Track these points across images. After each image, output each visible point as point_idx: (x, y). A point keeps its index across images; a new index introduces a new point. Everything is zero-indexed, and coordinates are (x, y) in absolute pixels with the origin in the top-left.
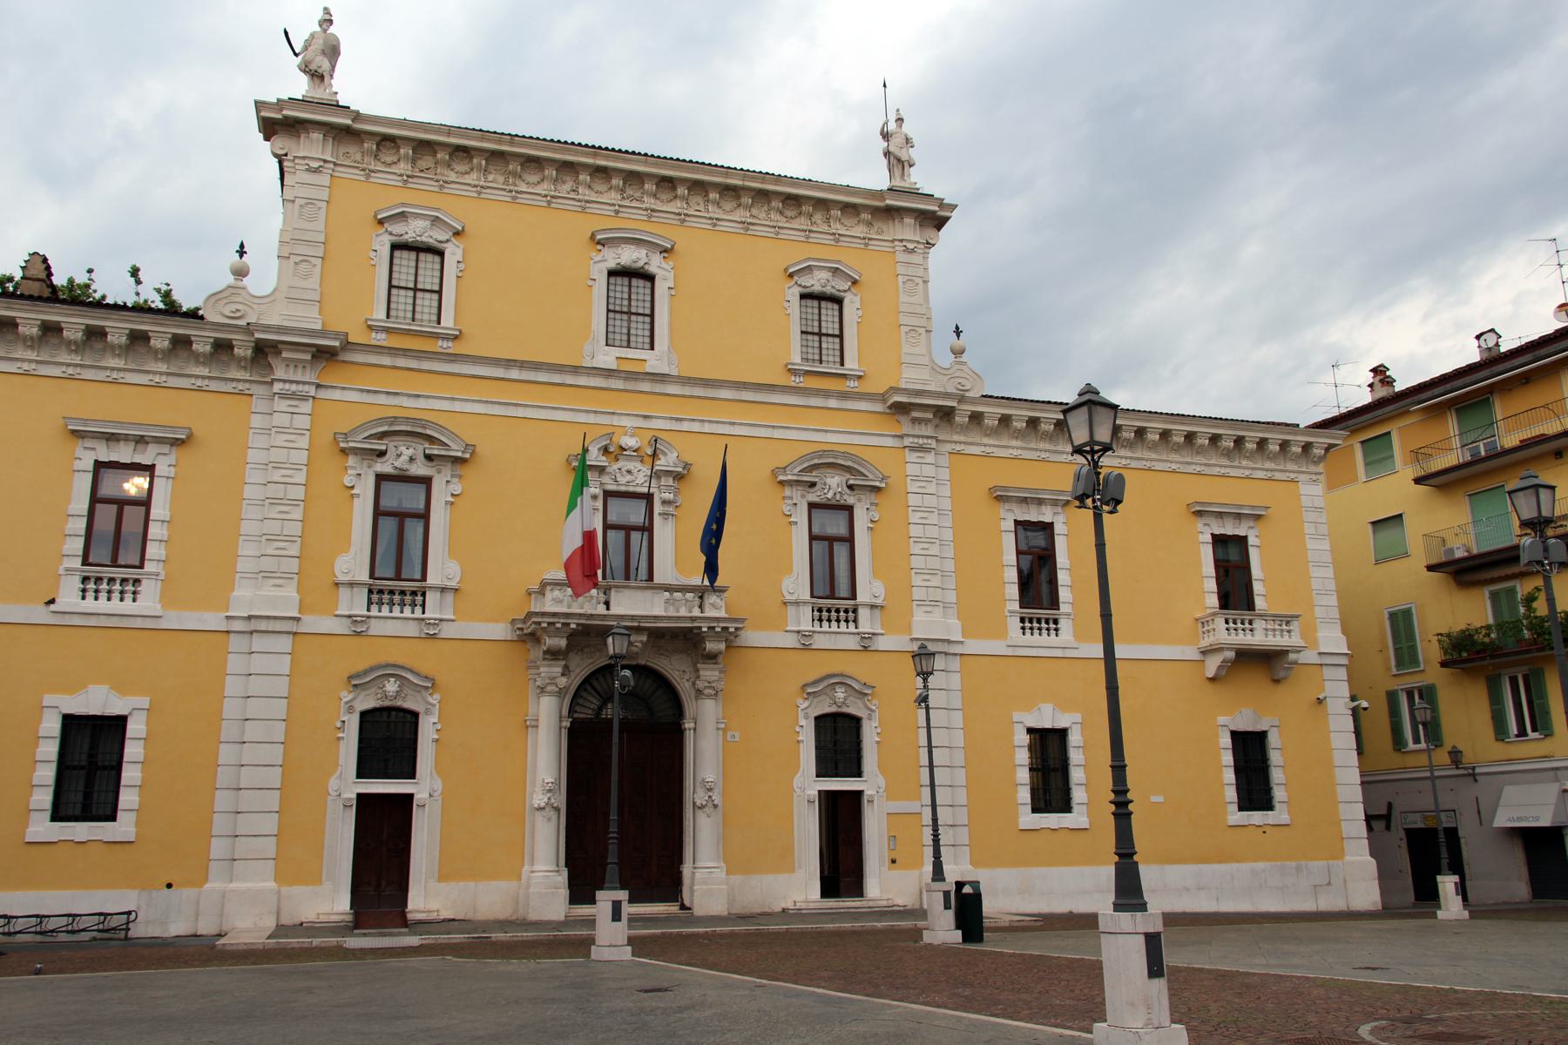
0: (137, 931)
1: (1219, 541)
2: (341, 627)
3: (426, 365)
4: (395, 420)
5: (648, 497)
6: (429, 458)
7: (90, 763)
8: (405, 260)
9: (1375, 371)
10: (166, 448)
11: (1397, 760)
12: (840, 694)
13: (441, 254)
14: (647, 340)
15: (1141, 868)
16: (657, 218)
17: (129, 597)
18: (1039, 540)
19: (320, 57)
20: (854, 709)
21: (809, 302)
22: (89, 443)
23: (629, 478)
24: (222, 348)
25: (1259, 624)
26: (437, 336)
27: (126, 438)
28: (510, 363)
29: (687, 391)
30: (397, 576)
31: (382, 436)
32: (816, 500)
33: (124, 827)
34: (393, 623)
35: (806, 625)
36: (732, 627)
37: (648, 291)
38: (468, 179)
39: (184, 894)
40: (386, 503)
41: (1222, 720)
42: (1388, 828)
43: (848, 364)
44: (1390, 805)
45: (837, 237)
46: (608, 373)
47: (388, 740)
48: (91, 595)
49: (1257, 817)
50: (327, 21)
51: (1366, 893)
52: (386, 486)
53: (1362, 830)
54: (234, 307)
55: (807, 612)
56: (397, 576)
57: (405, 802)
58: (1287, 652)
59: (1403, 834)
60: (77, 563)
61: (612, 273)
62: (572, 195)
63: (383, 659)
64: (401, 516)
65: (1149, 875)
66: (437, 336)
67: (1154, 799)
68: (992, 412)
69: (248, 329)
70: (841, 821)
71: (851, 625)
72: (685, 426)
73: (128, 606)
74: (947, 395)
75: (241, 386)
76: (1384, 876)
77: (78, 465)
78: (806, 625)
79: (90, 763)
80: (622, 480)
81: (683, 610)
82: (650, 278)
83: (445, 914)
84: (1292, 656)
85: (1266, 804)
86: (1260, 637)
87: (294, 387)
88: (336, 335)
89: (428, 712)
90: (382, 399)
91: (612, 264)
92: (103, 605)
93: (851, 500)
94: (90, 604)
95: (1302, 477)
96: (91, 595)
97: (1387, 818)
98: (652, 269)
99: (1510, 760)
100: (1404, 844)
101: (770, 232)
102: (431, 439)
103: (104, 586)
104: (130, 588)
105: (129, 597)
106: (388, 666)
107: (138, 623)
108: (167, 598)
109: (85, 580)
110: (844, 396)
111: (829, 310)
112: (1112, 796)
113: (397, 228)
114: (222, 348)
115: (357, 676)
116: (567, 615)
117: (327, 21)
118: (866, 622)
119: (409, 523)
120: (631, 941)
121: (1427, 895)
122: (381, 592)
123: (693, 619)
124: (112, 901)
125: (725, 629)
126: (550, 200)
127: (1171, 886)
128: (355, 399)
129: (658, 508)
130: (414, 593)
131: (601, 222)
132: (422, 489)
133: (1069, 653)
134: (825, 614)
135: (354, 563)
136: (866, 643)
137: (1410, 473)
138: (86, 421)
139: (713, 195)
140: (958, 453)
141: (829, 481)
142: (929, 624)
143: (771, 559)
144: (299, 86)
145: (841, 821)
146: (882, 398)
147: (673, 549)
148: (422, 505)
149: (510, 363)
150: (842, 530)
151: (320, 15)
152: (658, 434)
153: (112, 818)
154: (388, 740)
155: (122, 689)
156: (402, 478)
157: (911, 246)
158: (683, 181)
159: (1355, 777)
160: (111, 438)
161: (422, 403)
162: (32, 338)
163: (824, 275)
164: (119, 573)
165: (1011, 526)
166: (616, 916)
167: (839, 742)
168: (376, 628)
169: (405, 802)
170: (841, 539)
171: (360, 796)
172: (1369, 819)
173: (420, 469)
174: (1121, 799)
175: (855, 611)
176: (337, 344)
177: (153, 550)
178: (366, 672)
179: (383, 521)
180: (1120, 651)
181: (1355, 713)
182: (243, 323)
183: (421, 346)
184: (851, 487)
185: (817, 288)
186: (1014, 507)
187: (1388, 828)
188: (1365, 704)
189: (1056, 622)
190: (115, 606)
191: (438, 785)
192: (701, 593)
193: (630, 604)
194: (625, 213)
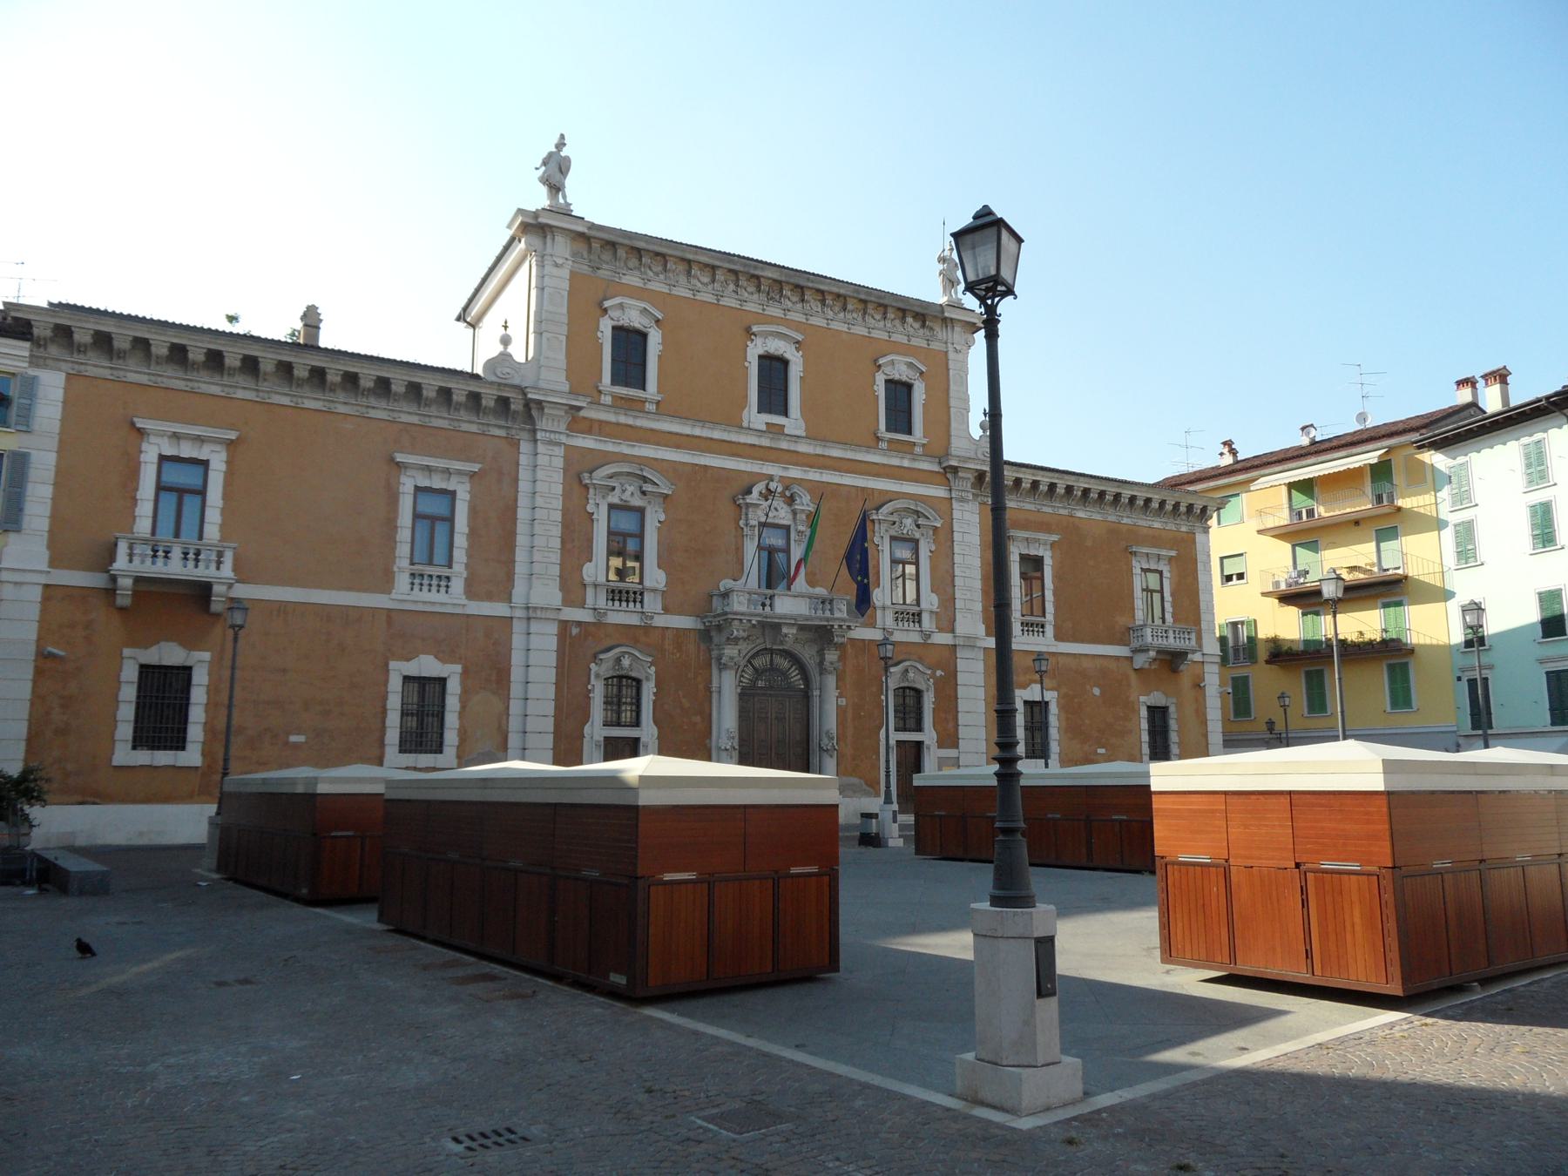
5: (788, 528)
9: (1225, 443)
17: (443, 590)
19: (555, 170)
24: (504, 402)
40: (421, 509)
41: (1142, 699)
48: (416, 587)
50: (561, 144)
52: (167, 466)
58: (1186, 654)
64: (181, 492)
68: (430, 386)
89: (648, 679)
92: (426, 596)
93: (917, 536)
96: (416, 587)
98: (787, 356)
99: (1306, 729)
102: (645, 480)
103: (426, 582)
104: (443, 583)
105: (443, 590)
108: (471, 592)
112: (996, 752)
116: (752, 615)
117: (561, 144)
123: (827, 620)
129: (793, 535)
132: (200, 469)
137: (1254, 525)
144: (539, 199)
148: (200, 482)
151: (556, 140)
155: (443, 657)
156: (623, 508)
162: (85, 346)
165: (412, 490)
170: (443, 519)
171: (606, 738)
173: (637, 502)
174: (1007, 755)
179: (164, 495)
184: (644, 493)
189: (448, 578)
190: (434, 596)
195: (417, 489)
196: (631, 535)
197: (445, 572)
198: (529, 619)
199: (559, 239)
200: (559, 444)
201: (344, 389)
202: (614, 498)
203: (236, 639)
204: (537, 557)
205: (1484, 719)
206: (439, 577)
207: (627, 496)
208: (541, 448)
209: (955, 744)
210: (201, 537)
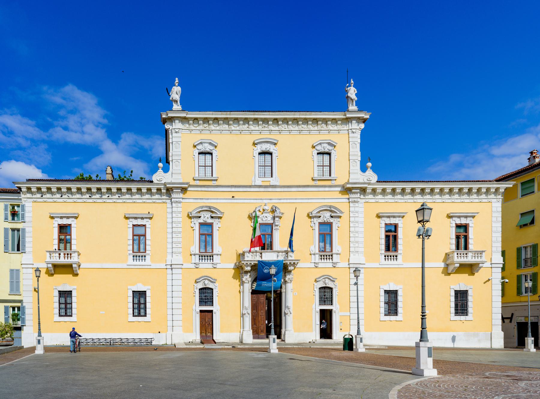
0: (154, 343)
1: (458, 226)
2: (193, 266)
3: (210, 189)
4: (202, 207)
6: (212, 217)
7: (139, 302)
8: (202, 157)
10: (73, 219)
11: (518, 299)
12: (207, 282)
13: (211, 154)
14: (270, 174)
15: (428, 333)
16: (273, 133)
18: (326, 229)
20: (211, 286)
21: (319, 156)
22: (131, 220)
23: (266, 219)
25: (470, 254)
26: (331, 180)
27: (139, 218)
28: (250, 186)
29: (282, 189)
30: (206, 250)
31: (319, 212)
32: (321, 221)
33: (148, 318)
34: (206, 265)
35: (197, 261)
36: (296, 262)
37: (270, 158)
38: (198, 128)
39: (163, 335)
42: (511, 322)
43: (214, 176)
44: (512, 314)
45: (329, 131)
46: (260, 186)
47: (206, 296)
48: (135, 260)
49: (393, 318)
51: (499, 342)
53: (500, 322)
54: (160, 177)
55: (317, 256)
56: (206, 250)
57: (330, 311)
59: (516, 324)
60: (131, 252)
61: (260, 154)
62: (247, 129)
63: (204, 275)
64: (139, 236)
65: (430, 335)
66: (331, 180)
67: (101, 312)
69: (165, 184)
70: (326, 316)
71: (331, 260)
72: (282, 201)
73: (143, 263)
74: (364, 183)
75: (164, 201)
76: (506, 338)
77: (54, 226)
78: (197, 261)
79: (139, 302)
80: (264, 219)
81: (281, 258)
82: (271, 154)
83: (222, 341)
84: (481, 265)
85: (396, 313)
86: (470, 259)
87: (177, 200)
88: (187, 184)
90: (199, 201)
91: (259, 151)
92: (138, 263)
93: (332, 220)
94: (135, 263)
95: (493, 200)
96: (135, 260)
97: (511, 319)
98: (271, 150)
100: (516, 327)
101: (307, 132)
102: (212, 212)
104: (143, 258)
106: (205, 276)
107: (146, 267)
109: (385, 256)
110: (330, 186)
111: (326, 157)
113: (200, 147)
114: (159, 190)
115: (198, 279)
118: (336, 258)
119: (142, 238)
120: (278, 348)
121: (521, 344)
122: (202, 256)
124: (149, 336)
125: (294, 263)
126: (241, 131)
127: (437, 339)
128: (191, 201)
130: (210, 256)
131: (256, 137)
133: (400, 266)
134: (323, 257)
135: (195, 249)
136: (334, 265)
138: (62, 214)
139: (241, 122)
140: (367, 202)
141: (325, 215)
142: (355, 259)
143: (308, 239)
145: (326, 316)
146: (343, 186)
147: (280, 241)
149: (250, 186)
150: (328, 232)
152: (276, 205)
153: (71, 316)
154: (206, 296)
157: (177, 130)
158: (280, 119)
159: (500, 305)
160: (136, 218)
161: (209, 201)
163: (206, 145)
164: (141, 254)
165: (131, 226)
166: (274, 342)
167: (326, 294)
168: (201, 266)
169: (330, 311)
172: (503, 319)
173: (210, 221)
175: (332, 256)
176: (187, 186)
177: (148, 248)
178: (200, 278)
180: (426, 265)
181: (503, 284)
182: (163, 182)
183: (209, 182)
185: (323, 150)
186: (133, 220)
187: (511, 322)
188: (507, 281)
189: (396, 256)
190: (141, 263)
191: (219, 308)
192: (287, 252)
193: (268, 256)
194: (263, 133)
195: (133, 225)
196: (142, 236)
197: (143, 254)
198: (172, 269)
199: (354, 122)
200: (180, 202)
201: (158, 194)
202: (201, 220)
203: (38, 280)
204: (174, 246)
205: (142, 311)
206: (139, 256)
207: (205, 219)
208: (174, 205)
209: (322, 312)
210: (71, 250)
